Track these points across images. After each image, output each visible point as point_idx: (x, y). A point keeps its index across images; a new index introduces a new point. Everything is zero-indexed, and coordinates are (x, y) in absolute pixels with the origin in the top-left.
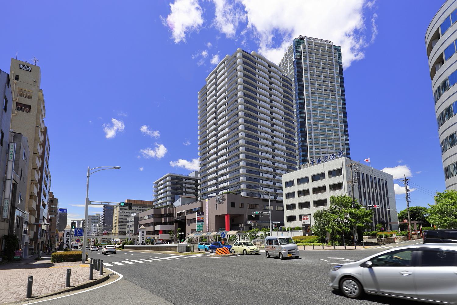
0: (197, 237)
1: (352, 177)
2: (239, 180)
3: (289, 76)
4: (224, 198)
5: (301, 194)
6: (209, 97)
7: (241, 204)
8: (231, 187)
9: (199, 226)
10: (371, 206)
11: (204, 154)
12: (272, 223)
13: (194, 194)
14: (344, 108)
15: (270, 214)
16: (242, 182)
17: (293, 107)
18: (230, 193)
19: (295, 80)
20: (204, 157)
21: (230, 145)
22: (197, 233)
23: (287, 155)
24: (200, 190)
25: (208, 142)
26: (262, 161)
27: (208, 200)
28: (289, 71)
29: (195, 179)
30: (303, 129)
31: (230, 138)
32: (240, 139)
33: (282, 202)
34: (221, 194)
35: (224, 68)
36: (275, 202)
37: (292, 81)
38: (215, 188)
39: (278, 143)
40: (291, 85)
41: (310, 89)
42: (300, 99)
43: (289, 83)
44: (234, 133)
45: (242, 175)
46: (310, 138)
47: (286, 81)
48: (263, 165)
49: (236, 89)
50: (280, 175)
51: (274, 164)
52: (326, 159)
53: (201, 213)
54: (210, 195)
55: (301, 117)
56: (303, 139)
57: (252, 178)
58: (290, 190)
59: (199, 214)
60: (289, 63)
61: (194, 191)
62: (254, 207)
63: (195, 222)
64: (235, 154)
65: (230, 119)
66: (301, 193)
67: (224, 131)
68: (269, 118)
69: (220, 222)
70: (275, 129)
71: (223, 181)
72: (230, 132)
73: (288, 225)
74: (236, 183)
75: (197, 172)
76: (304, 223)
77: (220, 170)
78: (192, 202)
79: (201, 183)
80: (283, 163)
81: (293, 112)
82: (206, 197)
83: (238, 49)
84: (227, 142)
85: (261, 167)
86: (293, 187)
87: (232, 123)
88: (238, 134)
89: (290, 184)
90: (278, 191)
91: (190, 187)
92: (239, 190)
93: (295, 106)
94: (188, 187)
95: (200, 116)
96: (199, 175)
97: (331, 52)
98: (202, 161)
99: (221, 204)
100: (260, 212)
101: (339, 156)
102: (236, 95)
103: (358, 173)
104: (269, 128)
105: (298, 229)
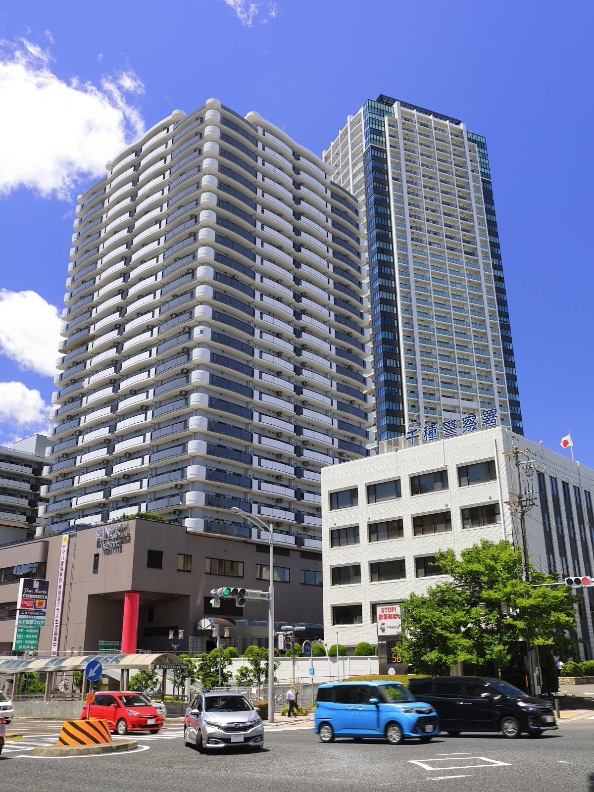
0: (12, 675)
1: (518, 488)
2: (183, 476)
3: (351, 187)
4: (125, 534)
5: (376, 532)
6: (110, 213)
7: (181, 558)
8: (154, 496)
9: (25, 633)
10: (581, 578)
11: (74, 381)
12: (278, 628)
13: (23, 514)
14: (501, 291)
15: (272, 599)
16: (192, 482)
17: (359, 269)
18: (150, 517)
19: (367, 199)
20: (74, 391)
21: (163, 361)
22: (15, 658)
23: (341, 406)
24: (46, 500)
25: (92, 346)
26: (260, 420)
27: (70, 537)
28: (351, 176)
29: (32, 462)
30: (389, 336)
31: (165, 341)
32: (195, 347)
33: (317, 556)
34: (119, 521)
35: (164, 142)
36: (299, 554)
37: (357, 201)
38: (98, 497)
39: (312, 369)
40: (356, 212)
41: (409, 230)
42: (381, 251)
43: (350, 206)
44: (178, 325)
45: (193, 460)
46: (411, 364)
47: (343, 200)
48: (265, 433)
49: (195, 203)
50: (316, 468)
51: (298, 430)
52: (450, 430)
53: (36, 585)
54: (80, 521)
55: (383, 301)
56: (391, 363)
57: (224, 471)
58: (342, 518)
59: (31, 587)
60: (352, 155)
61: (24, 503)
62: (225, 569)
63: (12, 615)
64: (177, 391)
65: (168, 284)
66: (378, 530)
67: (147, 318)
68: (289, 295)
69: (105, 620)
70: (305, 327)
71: (129, 476)
72: (166, 321)
73: (335, 635)
74: (172, 484)
75: (42, 442)
76: (383, 630)
77: (122, 437)
78: (12, 543)
79: (50, 477)
80: (327, 432)
81: (360, 284)
82: (63, 526)
83: (209, 101)
84: (154, 350)
85: (256, 437)
86: (352, 509)
87: (175, 297)
88: (189, 331)
89: (344, 498)
90: (308, 520)
91: (12, 490)
92: (180, 511)
93: (367, 267)
94: (6, 488)
95: (75, 265)
96: (48, 450)
97: (461, 145)
98: (65, 403)
99: (114, 556)
100: (236, 590)
101: (489, 421)
102: (195, 217)
103: (541, 476)
104: (289, 323)
105: (366, 651)
